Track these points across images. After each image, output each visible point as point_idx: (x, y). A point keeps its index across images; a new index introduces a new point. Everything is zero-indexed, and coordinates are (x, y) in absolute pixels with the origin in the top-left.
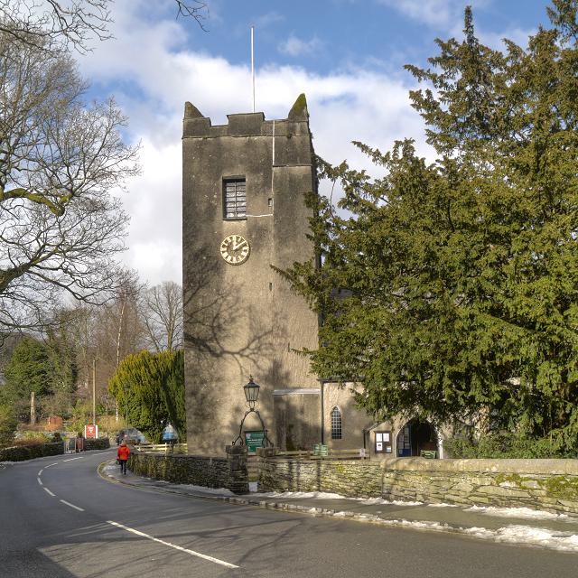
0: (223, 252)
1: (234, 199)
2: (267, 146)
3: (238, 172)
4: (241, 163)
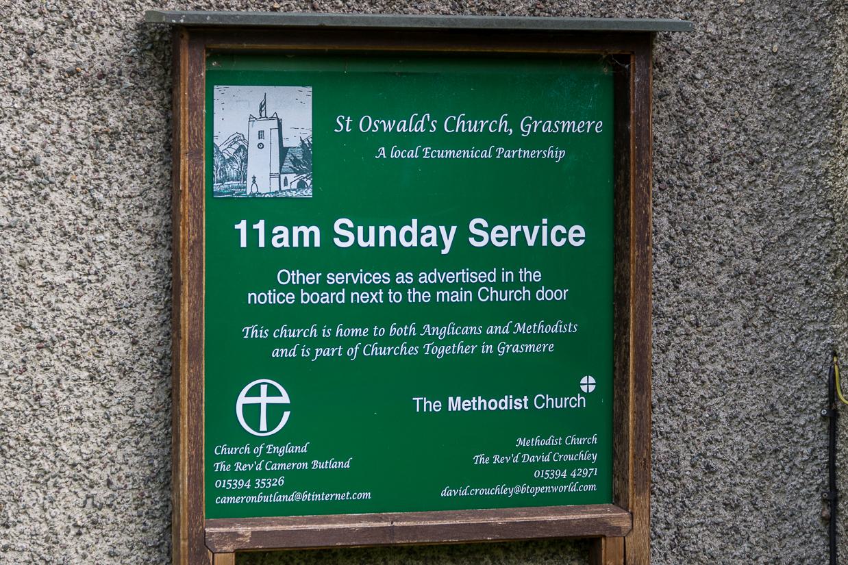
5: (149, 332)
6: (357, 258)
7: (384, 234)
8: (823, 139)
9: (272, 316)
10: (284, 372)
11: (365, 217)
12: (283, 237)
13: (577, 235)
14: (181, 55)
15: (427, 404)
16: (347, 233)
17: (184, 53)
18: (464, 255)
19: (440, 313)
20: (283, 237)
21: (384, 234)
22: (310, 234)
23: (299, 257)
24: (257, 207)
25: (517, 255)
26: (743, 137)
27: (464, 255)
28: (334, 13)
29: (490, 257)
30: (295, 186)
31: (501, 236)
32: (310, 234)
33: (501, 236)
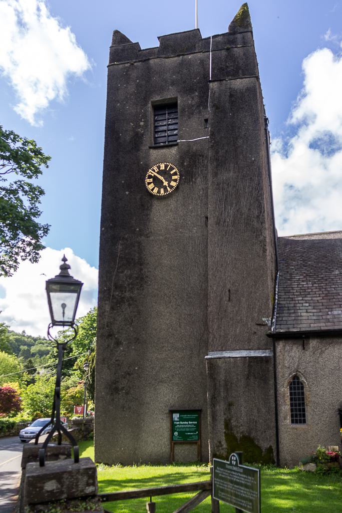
0: (149, 183)
1: (165, 128)
2: (203, 63)
3: (170, 94)
4: (173, 84)
5: (139, 171)
6: (182, 424)
7: (183, 423)
8: (80, 336)
9: (177, 428)
10: (177, 432)
11: (182, 422)
12: (177, 423)
13: (196, 423)
14: (160, 497)
15: (186, 434)
16: (181, 423)
17: (161, 498)
18: (189, 424)
19: (187, 428)
20: (177, 423)
21: (183, 423)
22: (179, 423)
23: (178, 424)
24: (176, 421)
25: (192, 424)
26: (239, 436)
27: (189, 424)
28: (309, 418)
29: (190, 424)
30: (178, 420)
31: (191, 423)
32: (179, 423)
33: (191, 423)
